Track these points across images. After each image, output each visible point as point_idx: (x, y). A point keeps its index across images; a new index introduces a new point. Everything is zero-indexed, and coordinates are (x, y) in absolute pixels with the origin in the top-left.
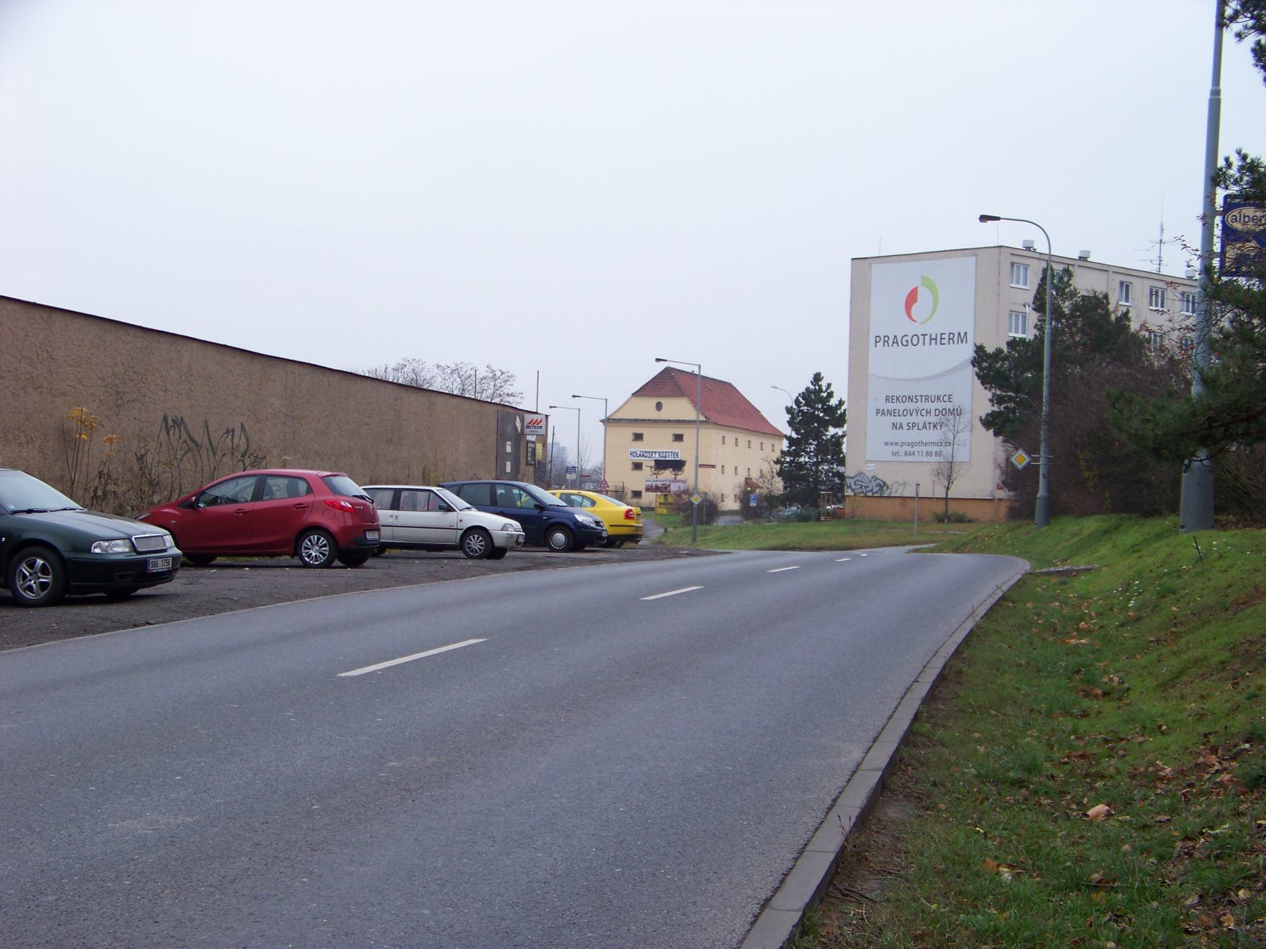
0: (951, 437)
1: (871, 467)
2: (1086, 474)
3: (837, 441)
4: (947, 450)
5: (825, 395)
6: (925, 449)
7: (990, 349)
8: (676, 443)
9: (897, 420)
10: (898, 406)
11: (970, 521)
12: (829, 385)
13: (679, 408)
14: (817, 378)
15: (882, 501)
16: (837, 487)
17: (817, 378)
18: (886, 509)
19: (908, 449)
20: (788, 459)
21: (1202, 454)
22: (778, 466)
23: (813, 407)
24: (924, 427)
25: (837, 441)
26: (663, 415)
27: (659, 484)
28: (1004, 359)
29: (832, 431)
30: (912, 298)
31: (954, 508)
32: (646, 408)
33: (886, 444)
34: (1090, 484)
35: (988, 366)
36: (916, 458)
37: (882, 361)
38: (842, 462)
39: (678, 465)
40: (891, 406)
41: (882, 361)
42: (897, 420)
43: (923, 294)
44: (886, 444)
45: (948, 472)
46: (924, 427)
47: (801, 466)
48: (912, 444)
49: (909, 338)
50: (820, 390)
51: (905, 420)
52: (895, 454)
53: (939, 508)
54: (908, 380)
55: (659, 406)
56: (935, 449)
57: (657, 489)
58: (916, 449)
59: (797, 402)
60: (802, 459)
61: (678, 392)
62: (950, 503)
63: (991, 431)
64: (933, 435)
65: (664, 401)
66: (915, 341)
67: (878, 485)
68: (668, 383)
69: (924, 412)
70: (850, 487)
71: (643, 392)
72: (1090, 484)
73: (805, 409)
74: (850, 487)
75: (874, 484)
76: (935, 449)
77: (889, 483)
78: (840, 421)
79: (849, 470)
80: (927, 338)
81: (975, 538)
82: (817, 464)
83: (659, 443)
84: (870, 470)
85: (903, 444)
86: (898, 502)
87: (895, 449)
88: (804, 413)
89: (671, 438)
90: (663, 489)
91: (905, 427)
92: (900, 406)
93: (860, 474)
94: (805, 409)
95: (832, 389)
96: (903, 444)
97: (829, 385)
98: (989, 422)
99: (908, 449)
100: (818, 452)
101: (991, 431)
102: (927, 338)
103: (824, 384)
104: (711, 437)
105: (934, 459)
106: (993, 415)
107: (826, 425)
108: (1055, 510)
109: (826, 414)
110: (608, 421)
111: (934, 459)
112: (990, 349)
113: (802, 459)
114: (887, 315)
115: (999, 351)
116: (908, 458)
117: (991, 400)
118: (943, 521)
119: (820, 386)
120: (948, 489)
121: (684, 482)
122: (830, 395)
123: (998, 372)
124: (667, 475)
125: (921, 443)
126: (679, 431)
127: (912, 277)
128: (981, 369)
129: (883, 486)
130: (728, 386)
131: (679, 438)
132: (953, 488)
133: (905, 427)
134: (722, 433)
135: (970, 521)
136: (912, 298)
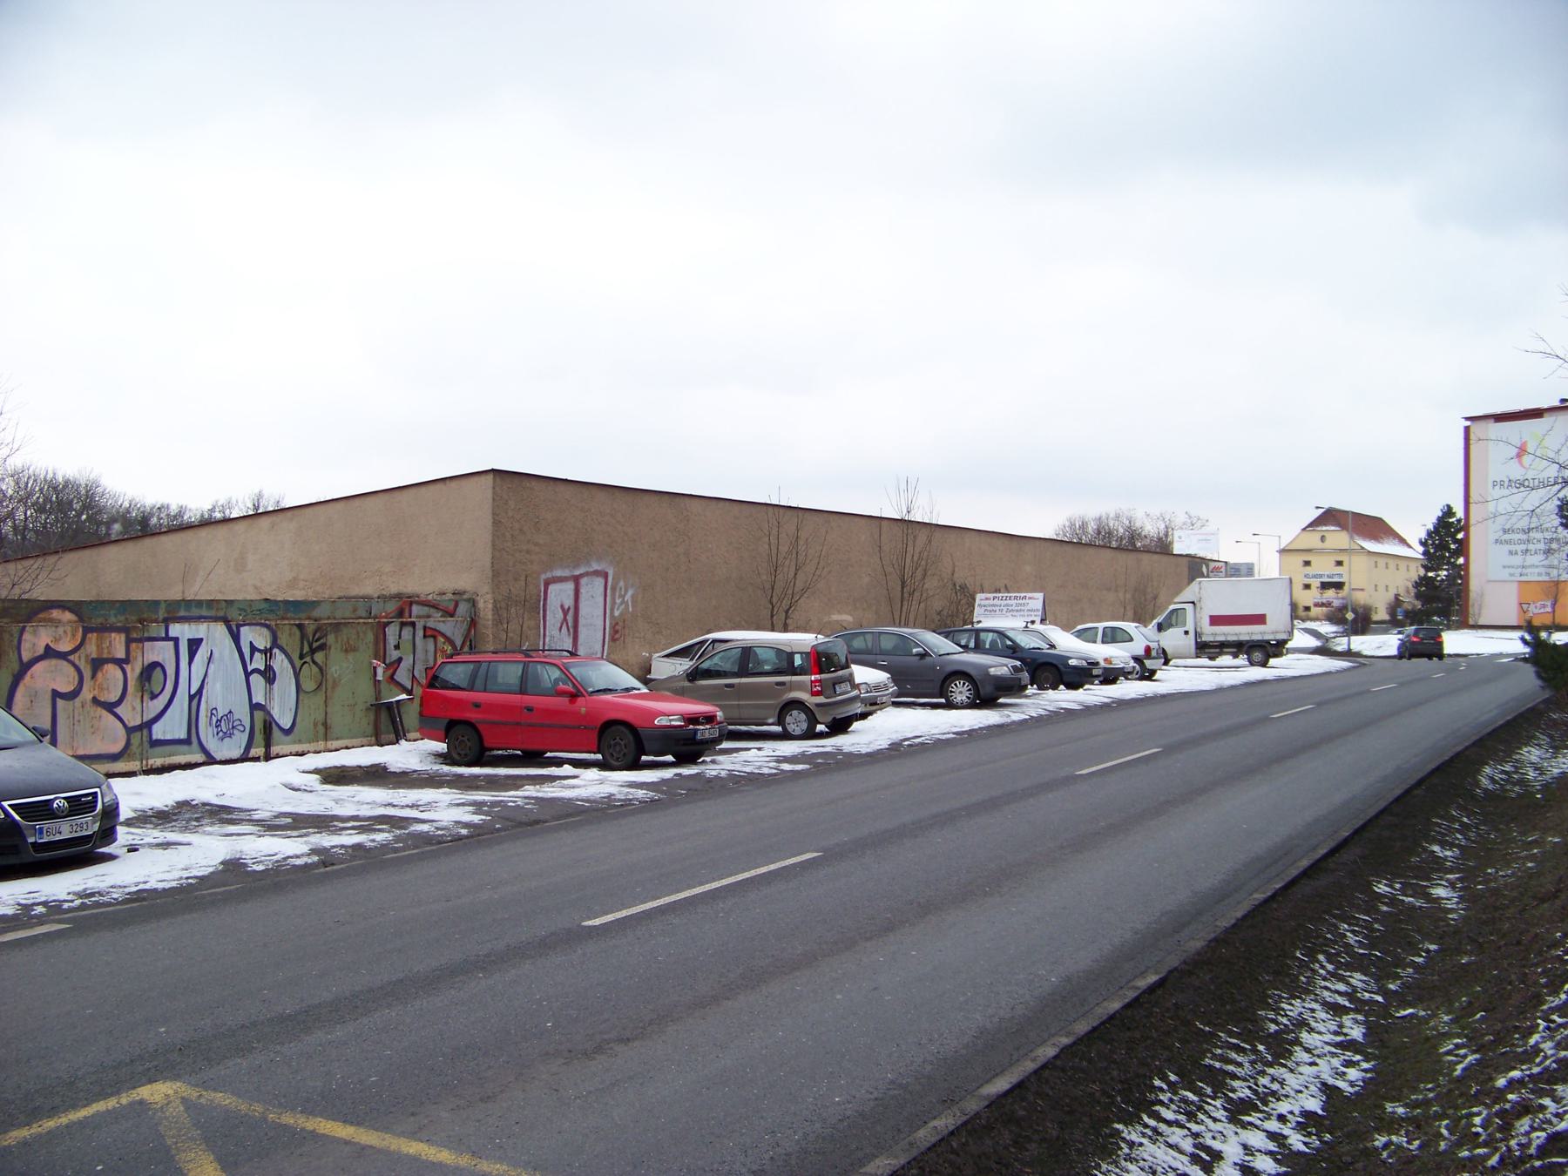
9: (1513, 548)
26: (1328, 544)
32: (1312, 540)
39: (1339, 586)
40: (1507, 537)
42: (1513, 548)
55: (1323, 539)
83: (1324, 568)
110: (1283, 551)
131: (1339, 563)
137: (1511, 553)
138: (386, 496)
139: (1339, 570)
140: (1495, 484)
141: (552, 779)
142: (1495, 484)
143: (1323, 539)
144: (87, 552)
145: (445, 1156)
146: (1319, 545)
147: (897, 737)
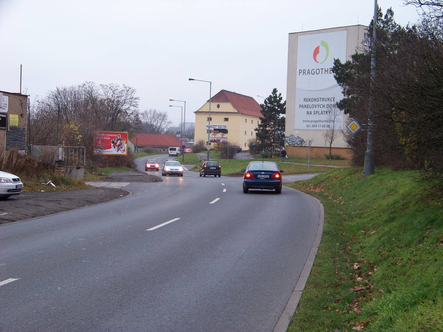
0: (333, 117)
1: (297, 132)
2: (403, 141)
3: (283, 120)
4: (332, 124)
5: (278, 99)
6: (322, 124)
7: (343, 62)
8: (226, 122)
9: (309, 110)
10: (309, 103)
11: (343, 159)
12: (280, 94)
13: (227, 107)
14: (275, 91)
15: (302, 148)
16: (281, 140)
17: (275, 91)
18: (303, 152)
19: (314, 124)
20: (261, 128)
21: (60, 158)
22: (257, 132)
23: (272, 105)
24: (322, 113)
25: (283, 120)
26: (220, 110)
27: (216, 139)
28: (351, 68)
29: (281, 115)
30: (316, 51)
31: (334, 152)
32: (214, 107)
33: (304, 121)
34: (407, 151)
35: (341, 72)
36: (317, 128)
37: (302, 82)
38: (284, 130)
39: (225, 131)
40: (306, 103)
41: (302, 82)
42: (309, 110)
43: (321, 49)
44: (304, 121)
45: (331, 136)
46: (322, 113)
47: (267, 132)
48: (316, 122)
49: (315, 71)
50: (276, 97)
51: (312, 110)
52: (308, 126)
53: (327, 152)
54: (316, 91)
55: (218, 106)
56: (326, 124)
57: (215, 141)
58: (318, 124)
59: (265, 102)
60: (267, 129)
61: (226, 100)
62: (332, 149)
63: (343, 111)
64: (324, 117)
65: (221, 104)
66: (318, 72)
67: (300, 141)
68: (223, 96)
69: (321, 106)
70: (287, 142)
71: (213, 99)
72: (407, 151)
73: (269, 105)
74: (287, 142)
75: (298, 140)
76: (326, 124)
77: (305, 140)
78: (284, 112)
79: (287, 133)
80: (324, 70)
81: (328, 177)
82: (274, 131)
83: (218, 122)
84: (296, 134)
85: (311, 121)
86: (308, 149)
87: (308, 123)
88: (269, 107)
89: (223, 119)
90: (217, 141)
91: (313, 113)
92: (311, 103)
93: (292, 135)
94: (269, 105)
95: (281, 96)
96: (311, 121)
97: (280, 94)
98: (342, 105)
99: (314, 124)
100: (275, 124)
101: (343, 111)
102: (324, 70)
103: (278, 94)
104: (240, 119)
105: (325, 128)
106: (344, 101)
107: (279, 113)
108: (377, 163)
109: (279, 108)
110: (197, 112)
111: (325, 128)
112: (343, 62)
113: (267, 129)
114: (305, 61)
115: (348, 63)
116: (314, 128)
117: (343, 93)
118: (328, 159)
119: (276, 95)
120: (331, 143)
121: (226, 138)
122: (281, 99)
123: (347, 74)
124: (219, 135)
125: (320, 121)
126: (227, 117)
127: (316, 41)
128: (337, 73)
129: (302, 141)
130: (252, 98)
131: (226, 119)
132: (333, 143)
133: (313, 113)
134: (245, 118)
135: (343, 159)
136: (316, 51)
137: (308, 113)
138: (13, 95)
139: (225, 123)
140: (300, 71)
141: (19, 194)
142: (300, 71)
143: (218, 106)
144: (346, 47)
145: (11, 280)
146: (216, 110)
147: (59, 95)
